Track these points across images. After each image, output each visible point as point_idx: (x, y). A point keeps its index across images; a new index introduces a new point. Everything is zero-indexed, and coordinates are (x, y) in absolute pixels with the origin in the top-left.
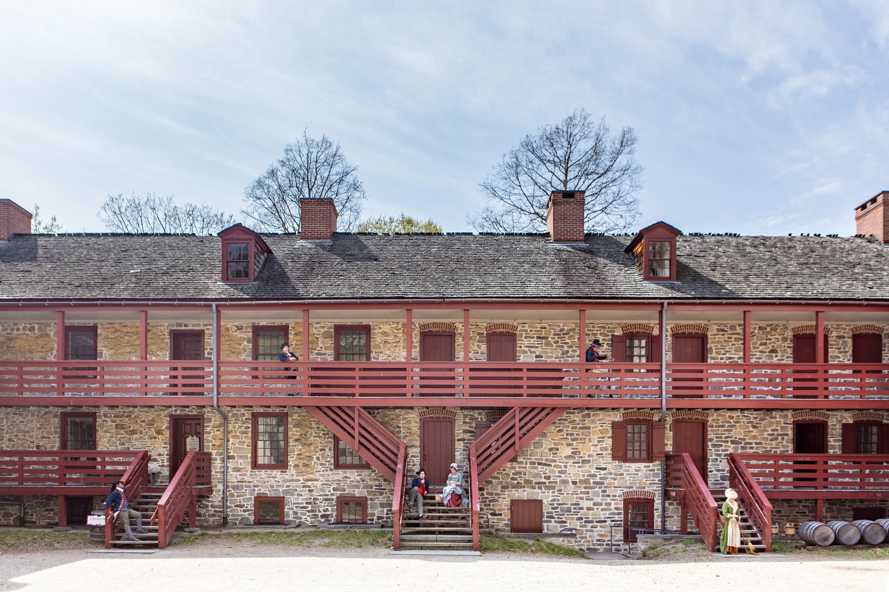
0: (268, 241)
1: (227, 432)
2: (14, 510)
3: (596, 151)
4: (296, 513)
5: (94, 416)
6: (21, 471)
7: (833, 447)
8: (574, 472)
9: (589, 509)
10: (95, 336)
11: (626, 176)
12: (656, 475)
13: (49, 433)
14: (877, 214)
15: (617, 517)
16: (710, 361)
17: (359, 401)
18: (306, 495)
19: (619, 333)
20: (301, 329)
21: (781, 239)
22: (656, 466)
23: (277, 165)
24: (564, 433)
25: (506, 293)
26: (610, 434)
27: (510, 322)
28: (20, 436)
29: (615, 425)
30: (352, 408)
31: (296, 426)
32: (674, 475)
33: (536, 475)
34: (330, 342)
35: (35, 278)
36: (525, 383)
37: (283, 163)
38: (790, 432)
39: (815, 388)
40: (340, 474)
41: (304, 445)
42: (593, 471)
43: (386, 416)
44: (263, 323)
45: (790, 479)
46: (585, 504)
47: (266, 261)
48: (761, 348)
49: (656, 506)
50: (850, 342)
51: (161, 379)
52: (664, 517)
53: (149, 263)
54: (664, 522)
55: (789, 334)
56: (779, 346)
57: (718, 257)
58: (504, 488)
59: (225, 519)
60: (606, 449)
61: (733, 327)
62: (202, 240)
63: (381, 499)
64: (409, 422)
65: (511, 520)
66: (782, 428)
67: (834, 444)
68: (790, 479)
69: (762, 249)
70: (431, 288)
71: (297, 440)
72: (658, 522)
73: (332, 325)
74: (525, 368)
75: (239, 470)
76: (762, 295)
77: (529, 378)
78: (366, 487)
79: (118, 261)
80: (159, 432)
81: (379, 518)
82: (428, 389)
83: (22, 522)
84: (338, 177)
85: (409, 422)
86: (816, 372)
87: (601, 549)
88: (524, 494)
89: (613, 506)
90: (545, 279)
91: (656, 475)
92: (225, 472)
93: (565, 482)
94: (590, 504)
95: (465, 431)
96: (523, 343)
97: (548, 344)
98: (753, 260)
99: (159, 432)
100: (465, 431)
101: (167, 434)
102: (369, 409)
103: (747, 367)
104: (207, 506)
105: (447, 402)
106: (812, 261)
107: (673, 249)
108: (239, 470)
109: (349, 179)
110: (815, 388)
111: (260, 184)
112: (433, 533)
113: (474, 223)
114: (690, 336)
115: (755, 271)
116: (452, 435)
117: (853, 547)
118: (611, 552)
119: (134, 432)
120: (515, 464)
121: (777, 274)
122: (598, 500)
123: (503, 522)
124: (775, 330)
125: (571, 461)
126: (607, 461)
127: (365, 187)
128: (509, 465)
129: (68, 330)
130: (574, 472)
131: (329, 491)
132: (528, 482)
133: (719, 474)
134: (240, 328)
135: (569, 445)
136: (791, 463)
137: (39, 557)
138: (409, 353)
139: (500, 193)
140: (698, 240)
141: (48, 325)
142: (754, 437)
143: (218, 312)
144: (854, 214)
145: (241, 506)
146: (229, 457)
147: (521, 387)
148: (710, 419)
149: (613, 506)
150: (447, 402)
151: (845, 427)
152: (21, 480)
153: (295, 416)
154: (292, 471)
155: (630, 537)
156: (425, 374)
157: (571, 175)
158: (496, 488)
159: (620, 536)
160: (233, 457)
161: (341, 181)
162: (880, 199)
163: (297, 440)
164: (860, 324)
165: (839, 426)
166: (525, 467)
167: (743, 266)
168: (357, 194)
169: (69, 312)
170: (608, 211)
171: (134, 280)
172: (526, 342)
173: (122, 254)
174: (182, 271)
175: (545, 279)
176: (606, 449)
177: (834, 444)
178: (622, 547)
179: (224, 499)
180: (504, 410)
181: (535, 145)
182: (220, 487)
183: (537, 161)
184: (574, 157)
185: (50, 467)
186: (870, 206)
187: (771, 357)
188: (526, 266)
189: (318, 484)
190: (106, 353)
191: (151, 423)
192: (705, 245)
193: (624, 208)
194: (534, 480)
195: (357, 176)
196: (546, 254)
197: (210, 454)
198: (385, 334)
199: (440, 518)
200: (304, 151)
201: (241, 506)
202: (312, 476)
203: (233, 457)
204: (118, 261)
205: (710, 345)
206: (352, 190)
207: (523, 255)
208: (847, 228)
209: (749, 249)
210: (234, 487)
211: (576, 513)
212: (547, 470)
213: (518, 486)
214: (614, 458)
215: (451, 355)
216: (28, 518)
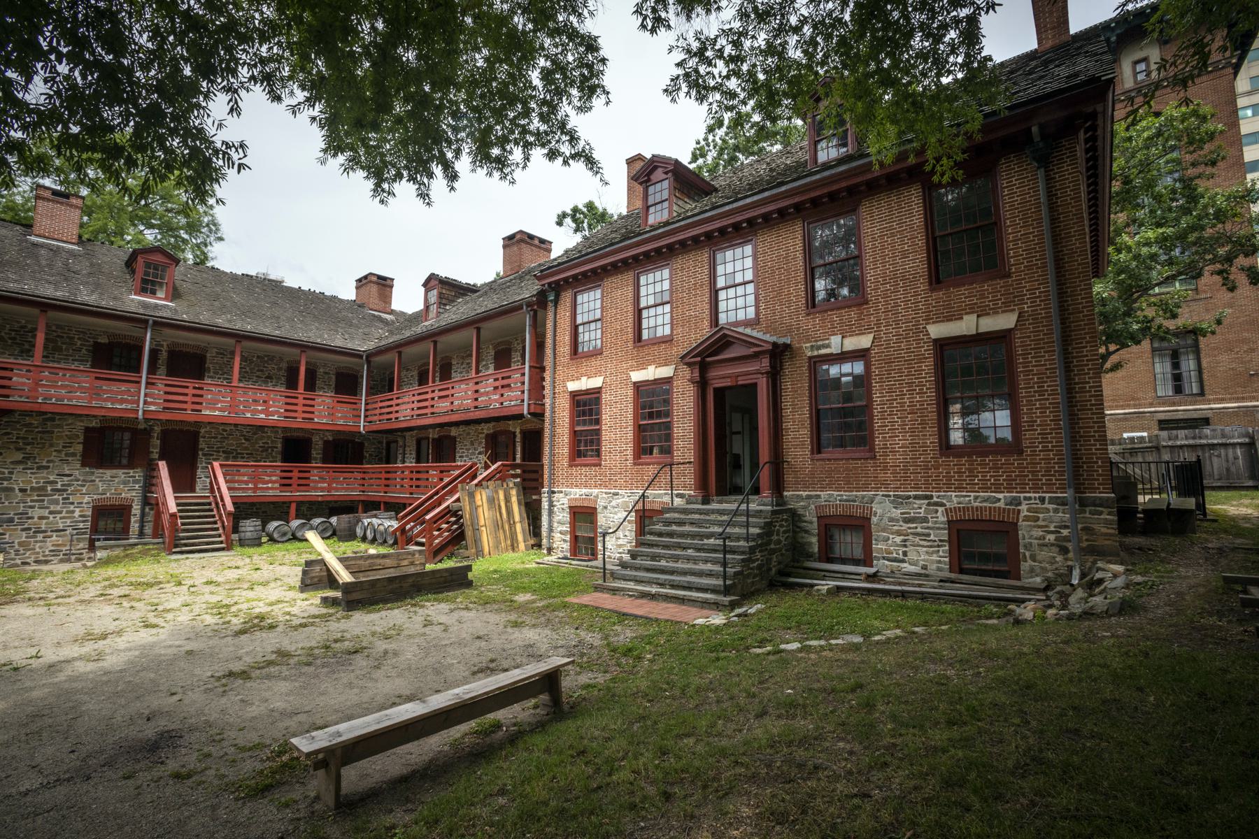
7: (316, 458)
12: (136, 482)
19: (103, 340)
26: (81, 439)
38: (279, 445)
45: (277, 485)
49: (133, 512)
50: (334, 377)
55: (284, 365)
66: (272, 441)
68: (277, 485)
89: (77, 514)
142: (246, 448)
144: (354, 284)
149: (77, 514)
151: (326, 443)
177: (316, 452)
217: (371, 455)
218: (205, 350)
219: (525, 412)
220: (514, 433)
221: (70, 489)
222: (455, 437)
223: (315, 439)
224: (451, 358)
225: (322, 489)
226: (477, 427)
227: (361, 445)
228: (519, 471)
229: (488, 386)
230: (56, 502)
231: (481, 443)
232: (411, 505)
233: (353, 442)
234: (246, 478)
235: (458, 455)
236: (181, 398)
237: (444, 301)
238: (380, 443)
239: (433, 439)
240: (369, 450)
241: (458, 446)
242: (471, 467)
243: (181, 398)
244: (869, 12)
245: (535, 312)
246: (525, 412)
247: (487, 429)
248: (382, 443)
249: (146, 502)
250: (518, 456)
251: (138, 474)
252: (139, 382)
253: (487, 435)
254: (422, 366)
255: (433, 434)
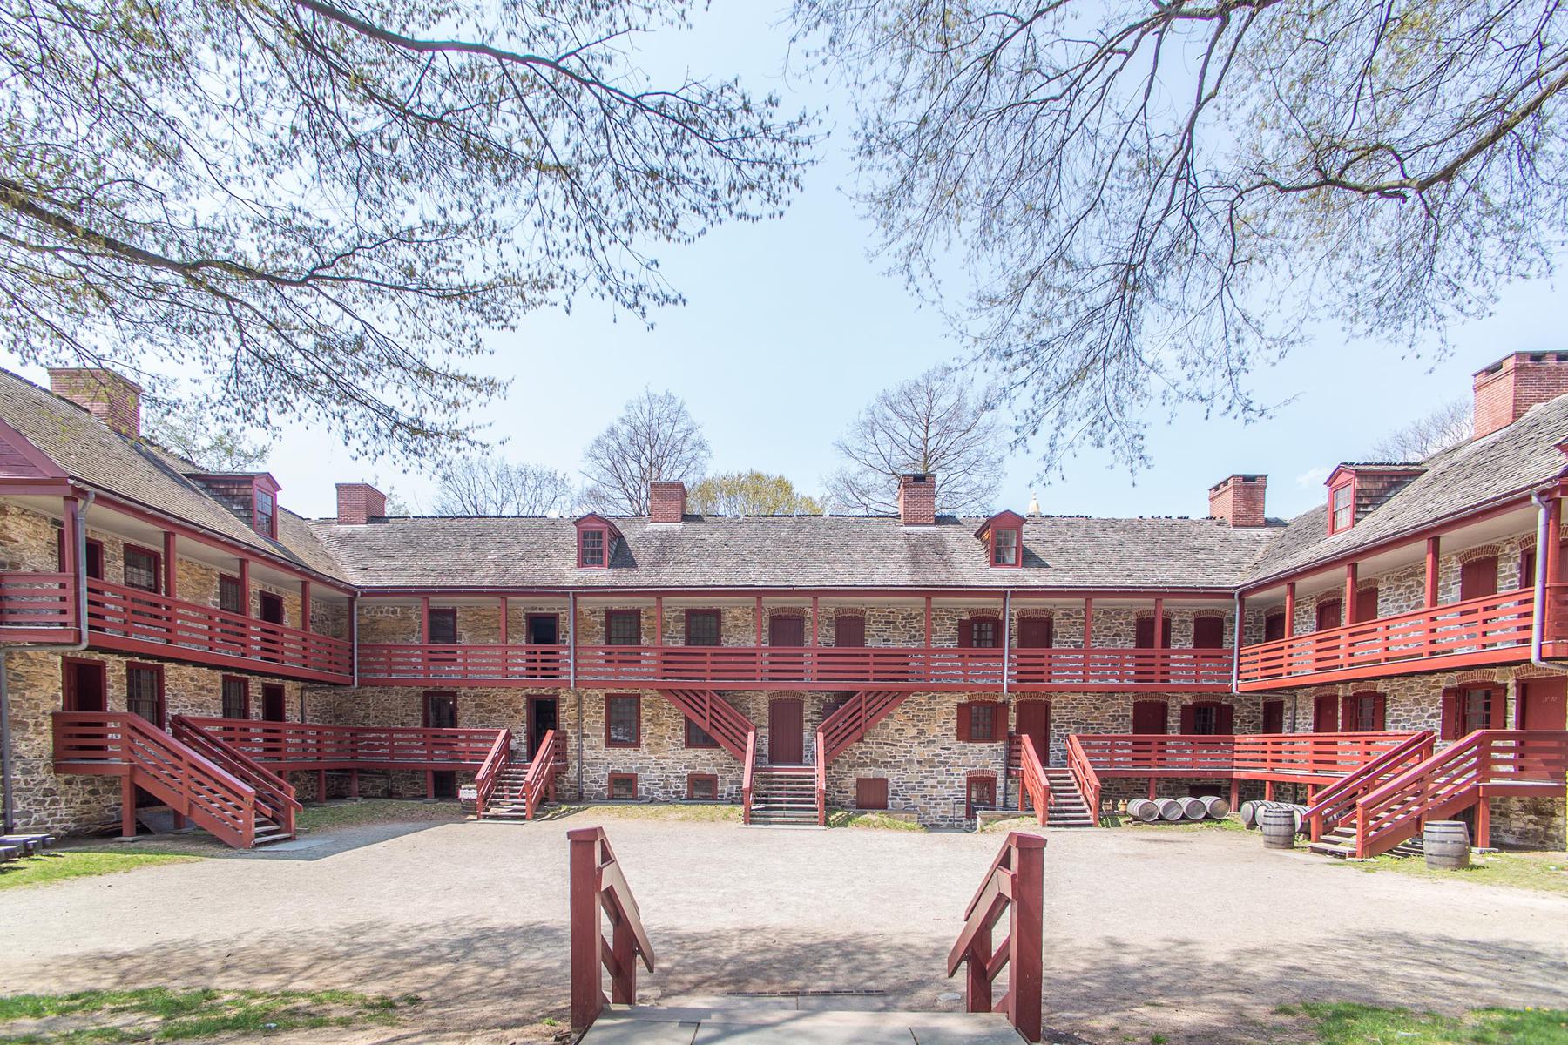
0: (618, 524)
1: (581, 712)
2: (381, 783)
3: (959, 407)
4: (648, 789)
5: (454, 695)
6: (391, 747)
7: (1172, 728)
8: (920, 752)
9: (933, 787)
10: (455, 618)
11: (989, 436)
12: (999, 755)
13: (412, 710)
14: (1228, 497)
15: (960, 795)
16: (1055, 646)
17: (710, 685)
18: (658, 772)
19: (965, 617)
20: (654, 614)
21: (1131, 522)
22: (1000, 746)
23: (617, 423)
24: (910, 714)
25: (855, 581)
26: (955, 716)
27: (859, 607)
28: (385, 713)
29: (960, 706)
30: (704, 692)
31: (648, 706)
32: (1016, 754)
33: (881, 755)
34: (681, 626)
35: (399, 564)
36: (871, 668)
37: (623, 421)
38: (1131, 714)
39: (1152, 673)
40: (691, 752)
41: (655, 724)
42: (938, 751)
43: (736, 697)
44: (615, 607)
45: (1129, 759)
46: (929, 782)
47: (618, 547)
48: (1105, 632)
49: (998, 784)
50: (1192, 625)
51: (519, 664)
52: (1006, 794)
53: (506, 548)
54: (1005, 800)
55: (1133, 618)
56: (1123, 630)
57: (1065, 542)
58: (851, 767)
59: (581, 793)
60: (951, 730)
61: (1078, 612)
62: (554, 523)
63: (731, 777)
64: (758, 703)
65: (857, 797)
66: (1123, 709)
67: (1174, 722)
68: (1129, 759)
69: (1110, 532)
70: (782, 576)
71: (649, 720)
72: (999, 799)
73: (683, 609)
74: (871, 653)
75: (593, 748)
76: (1104, 584)
77: (875, 664)
78: (716, 765)
79: (475, 546)
80: (517, 711)
81: (729, 795)
82: (776, 674)
83: (389, 794)
84: (682, 435)
85: (758, 703)
86: (1153, 657)
87: (944, 824)
88: (870, 773)
89: (956, 785)
90: (892, 566)
91: (999, 755)
92: (580, 750)
93: (910, 761)
94: (934, 782)
95: (813, 713)
96: (871, 628)
97: (896, 628)
98: (1100, 545)
99: (517, 711)
100: (813, 713)
101: (524, 713)
102: (720, 693)
103: (1088, 651)
104: (563, 782)
105: (795, 686)
106: (1157, 545)
107: (1019, 538)
108: (593, 748)
109: (694, 437)
110: (1152, 673)
111: (599, 442)
112: (781, 809)
113: (826, 483)
114: (1036, 620)
115: (1099, 557)
116: (801, 717)
117: (1176, 823)
118: (954, 826)
119: (492, 711)
120: (861, 744)
121: (1121, 561)
122: (941, 778)
123: (852, 794)
124: (1119, 614)
125: (917, 741)
126: (952, 742)
127: (712, 446)
128: (855, 745)
129: (433, 612)
130: (920, 752)
131: (680, 769)
132: (875, 762)
133: (1060, 753)
134: (593, 612)
135: (915, 726)
136: (1130, 743)
137: (348, 831)
138: (759, 637)
139: (856, 454)
140: (1048, 522)
141: (410, 608)
142: (1096, 718)
143: (575, 599)
144: (1208, 494)
145: (596, 782)
146: (584, 736)
147: (868, 672)
148: (1053, 701)
149: (956, 785)
150: (795, 686)
151: (1184, 707)
152: (391, 755)
153: (647, 697)
154: (644, 749)
155: (971, 814)
156: (775, 659)
157: (932, 432)
158: (841, 767)
159: (962, 812)
160: (588, 736)
161: (685, 439)
162: (1231, 482)
163: (649, 720)
164: (1202, 608)
165: (1179, 707)
166: (870, 746)
167: (1089, 552)
168: (702, 453)
169: (432, 599)
170: (970, 471)
171: (492, 566)
172: (874, 627)
173: (478, 538)
174: (538, 557)
175: (892, 566)
176: (951, 730)
177: (1174, 722)
178: (964, 823)
179: (580, 775)
180: (851, 694)
181: (893, 400)
182: (576, 764)
183: (895, 417)
184: (936, 413)
185: (415, 744)
186: (1222, 489)
187: (1114, 641)
188: (875, 552)
189: (670, 762)
190: (465, 638)
191: (509, 702)
192: (1054, 528)
193: (988, 468)
194: (880, 760)
195: (706, 433)
196: (895, 538)
197: (566, 732)
198: (735, 618)
199: (788, 795)
200: (646, 407)
201: (596, 782)
202: (663, 755)
203: (588, 736)
204: (475, 546)
205: (1056, 629)
206: (697, 448)
207: (873, 540)
208: (1199, 509)
209: (1098, 533)
210: (589, 765)
211: (921, 791)
212: (893, 750)
213: (865, 765)
214: (958, 739)
215: (800, 641)
216: (395, 790)
217: (1242, 721)
218: (1052, 613)
219: (1534, 657)
220: (1504, 687)
221: (951, 761)
222: (1385, 695)
223: (1172, 703)
224: (1376, 581)
225: (1181, 765)
226: (1427, 678)
227: (1231, 708)
228: (1512, 743)
229: (1449, 621)
230: (941, 773)
231: (1434, 701)
232: (1326, 786)
233: (1219, 705)
234: (1097, 751)
235: (1389, 720)
236: (1038, 669)
237: (1365, 501)
238: (1257, 704)
239: (1345, 699)
240: (1240, 713)
241: (1390, 707)
242: (1423, 737)
243: (1038, 669)
244: (1565, 967)
245: (1558, 502)
246: (1534, 657)
247: (1444, 681)
248: (1258, 704)
249: (1008, 774)
250: (1512, 720)
251: (1000, 746)
252: (1003, 656)
253: (1446, 692)
254: (1328, 594)
255: (831, 604)
